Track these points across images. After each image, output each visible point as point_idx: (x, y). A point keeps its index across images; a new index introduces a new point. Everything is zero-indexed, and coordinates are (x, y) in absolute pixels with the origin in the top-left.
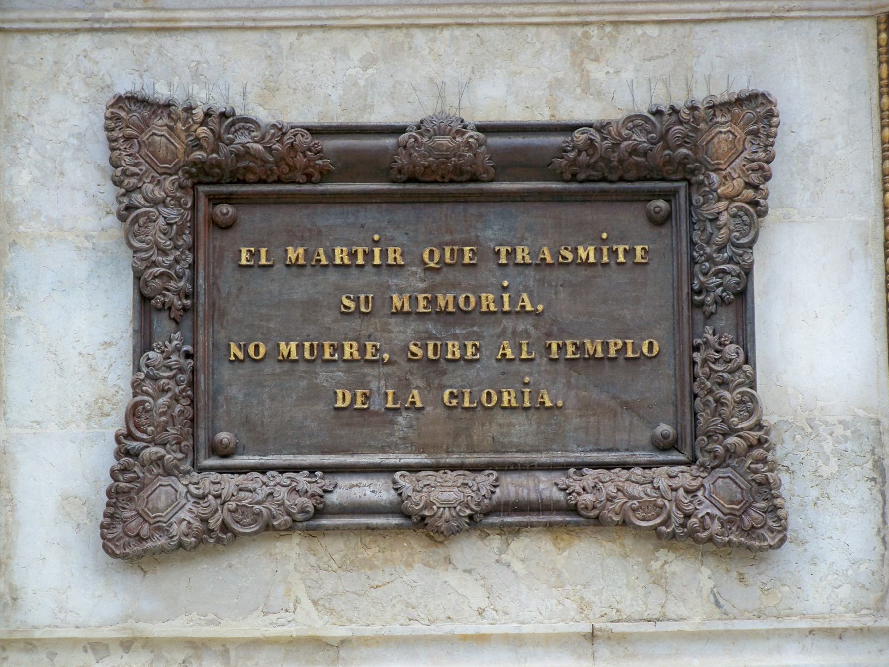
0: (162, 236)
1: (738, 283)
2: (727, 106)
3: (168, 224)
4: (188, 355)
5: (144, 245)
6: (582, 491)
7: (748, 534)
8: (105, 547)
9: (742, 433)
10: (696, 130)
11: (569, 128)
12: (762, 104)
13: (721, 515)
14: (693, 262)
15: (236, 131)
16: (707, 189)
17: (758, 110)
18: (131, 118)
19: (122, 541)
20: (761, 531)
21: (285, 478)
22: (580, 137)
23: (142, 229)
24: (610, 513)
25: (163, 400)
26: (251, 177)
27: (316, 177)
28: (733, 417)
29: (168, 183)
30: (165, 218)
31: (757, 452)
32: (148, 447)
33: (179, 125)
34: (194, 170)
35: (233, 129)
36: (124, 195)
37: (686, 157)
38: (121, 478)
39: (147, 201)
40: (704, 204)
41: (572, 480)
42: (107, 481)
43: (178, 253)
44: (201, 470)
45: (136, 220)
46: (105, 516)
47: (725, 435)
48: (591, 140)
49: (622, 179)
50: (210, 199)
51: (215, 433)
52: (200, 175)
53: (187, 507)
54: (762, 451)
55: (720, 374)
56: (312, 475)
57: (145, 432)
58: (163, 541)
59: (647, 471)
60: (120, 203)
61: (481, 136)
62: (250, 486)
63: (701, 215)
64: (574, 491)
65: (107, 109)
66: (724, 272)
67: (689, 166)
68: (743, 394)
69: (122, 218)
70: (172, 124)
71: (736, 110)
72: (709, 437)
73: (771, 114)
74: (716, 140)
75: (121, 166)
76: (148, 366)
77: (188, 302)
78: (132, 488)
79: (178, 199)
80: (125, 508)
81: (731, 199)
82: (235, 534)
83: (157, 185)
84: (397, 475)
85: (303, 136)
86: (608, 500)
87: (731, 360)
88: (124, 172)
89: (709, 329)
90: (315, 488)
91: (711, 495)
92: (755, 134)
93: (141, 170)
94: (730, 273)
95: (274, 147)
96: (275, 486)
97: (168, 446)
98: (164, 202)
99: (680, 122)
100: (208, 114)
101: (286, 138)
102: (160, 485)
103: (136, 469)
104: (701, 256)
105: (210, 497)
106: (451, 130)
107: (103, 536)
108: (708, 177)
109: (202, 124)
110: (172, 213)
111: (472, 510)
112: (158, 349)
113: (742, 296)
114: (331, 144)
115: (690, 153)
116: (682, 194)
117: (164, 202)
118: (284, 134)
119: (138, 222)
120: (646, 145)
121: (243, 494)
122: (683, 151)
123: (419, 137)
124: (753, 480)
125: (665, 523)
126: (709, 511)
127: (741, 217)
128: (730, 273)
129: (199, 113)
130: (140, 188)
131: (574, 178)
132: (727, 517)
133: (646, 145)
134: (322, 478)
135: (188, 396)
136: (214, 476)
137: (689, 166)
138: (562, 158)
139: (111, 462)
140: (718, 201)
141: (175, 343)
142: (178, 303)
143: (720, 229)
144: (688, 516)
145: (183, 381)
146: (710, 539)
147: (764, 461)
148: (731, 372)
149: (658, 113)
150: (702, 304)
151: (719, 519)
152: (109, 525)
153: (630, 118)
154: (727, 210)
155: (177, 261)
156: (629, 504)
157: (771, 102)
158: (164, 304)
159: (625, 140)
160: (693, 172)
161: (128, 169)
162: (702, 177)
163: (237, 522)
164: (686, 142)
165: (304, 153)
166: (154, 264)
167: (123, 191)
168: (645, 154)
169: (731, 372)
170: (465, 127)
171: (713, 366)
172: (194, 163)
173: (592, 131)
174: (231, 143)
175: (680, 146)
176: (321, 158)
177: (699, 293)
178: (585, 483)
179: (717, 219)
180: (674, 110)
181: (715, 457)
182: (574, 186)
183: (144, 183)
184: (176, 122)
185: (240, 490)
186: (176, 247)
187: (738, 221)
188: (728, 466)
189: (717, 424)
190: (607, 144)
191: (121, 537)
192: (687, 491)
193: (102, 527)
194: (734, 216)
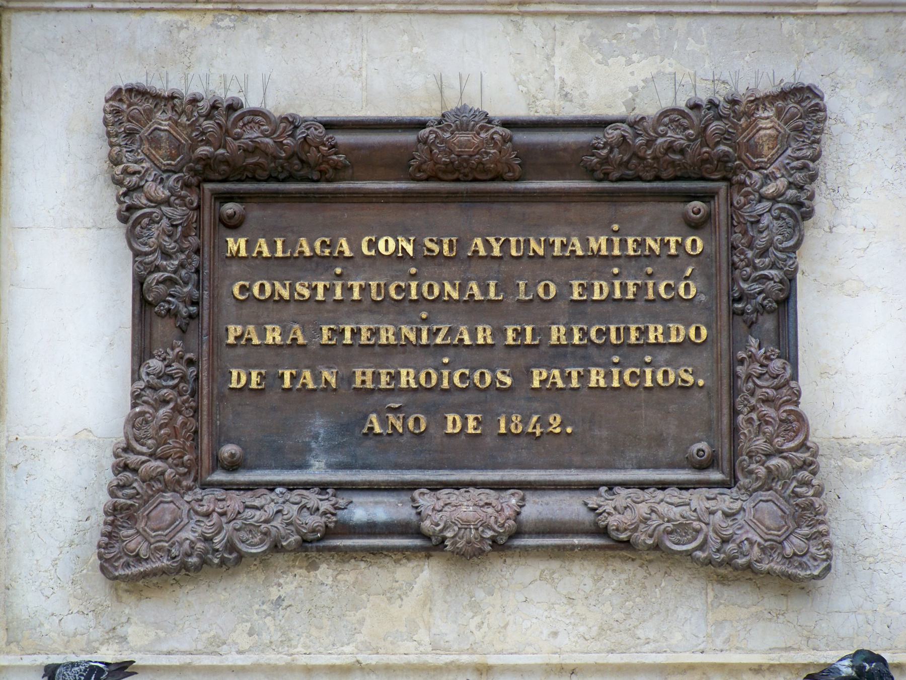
0: (167, 239)
1: (780, 290)
2: (771, 99)
3: (172, 225)
4: (190, 363)
5: (147, 249)
6: (612, 511)
7: (790, 562)
8: (103, 569)
9: (785, 454)
10: (735, 126)
11: (599, 124)
12: (808, 98)
13: (762, 542)
14: (733, 266)
15: (244, 125)
16: (750, 189)
17: (804, 104)
18: (131, 113)
19: (122, 561)
20: (805, 559)
21: (294, 496)
22: (612, 134)
23: (145, 231)
24: (643, 538)
25: (164, 411)
26: (260, 173)
27: (331, 173)
28: (778, 436)
29: (171, 182)
30: (169, 219)
31: (804, 474)
32: (149, 461)
33: (184, 119)
34: (199, 167)
35: (241, 124)
36: (125, 194)
37: (726, 154)
38: (120, 494)
39: (151, 201)
40: (745, 205)
41: (602, 499)
42: (104, 498)
43: (183, 257)
44: (205, 486)
45: (137, 222)
46: (103, 535)
47: (769, 456)
48: (623, 136)
49: (658, 178)
50: (216, 199)
51: (220, 445)
52: (205, 171)
53: (190, 526)
54: (806, 473)
55: (764, 390)
56: (324, 492)
57: (143, 445)
58: (166, 562)
59: (684, 492)
60: (120, 202)
61: (508, 131)
62: (257, 503)
63: (742, 216)
64: (604, 511)
65: (107, 101)
66: (766, 278)
67: (730, 165)
68: (790, 412)
69: (123, 219)
70: (176, 117)
71: (780, 103)
72: (751, 457)
73: (819, 109)
74: (757, 136)
75: (122, 163)
76: (148, 374)
77: (193, 309)
78: (132, 505)
79: (182, 198)
80: (123, 527)
81: (774, 199)
82: (241, 557)
83: (160, 183)
84: (416, 493)
85: (316, 129)
86: (641, 521)
87: (778, 375)
88: (125, 172)
89: (754, 342)
90: (325, 506)
91: (740, 515)
92: (799, 130)
93: (143, 167)
94: (772, 279)
95: (285, 142)
96: (284, 503)
97: (170, 460)
98: (167, 202)
99: (719, 117)
100: (214, 107)
101: (298, 131)
102: (161, 502)
103: (135, 485)
104: (742, 260)
105: (215, 515)
106: (474, 126)
107: (100, 557)
108: (750, 176)
109: (208, 116)
110: (177, 213)
111: (494, 531)
112: (159, 356)
113: (784, 303)
114: (341, 138)
115: (731, 150)
116: (723, 193)
117: (167, 202)
118: (296, 127)
119: (140, 223)
120: (682, 142)
121: (249, 513)
122: (722, 148)
123: (440, 132)
124: (797, 505)
125: (701, 547)
126: (750, 536)
127: (784, 219)
128: (772, 279)
129: (204, 106)
130: (143, 186)
131: (606, 177)
132: (769, 543)
133: (682, 142)
134: (334, 495)
135: (191, 407)
136: (219, 493)
137: (730, 165)
138: (593, 155)
139: (109, 477)
140: (760, 202)
141: (177, 350)
142: (184, 311)
143: (761, 232)
144: (725, 541)
145: (186, 391)
146: (749, 566)
147: (807, 484)
148: (777, 388)
149: (696, 107)
150: (743, 312)
151: (759, 544)
152: (107, 544)
153: (665, 113)
154: (769, 211)
155: (182, 266)
156: (662, 527)
157: (817, 96)
158: (169, 310)
159: (663, 136)
160: (736, 170)
161: (128, 167)
162: (742, 177)
163: (243, 542)
164: (726, 139)
165: (317, 148)
166: (158, 269)
167: (125, 189)
168: (682, 151)
169: (777, 388)
170: (490, 122)
171: (758, 382)
172: (199, 159)
173: (625, 126)
174: (239, 138)
175: (718, 143)
176: (336, 154)
177: (739, 300)
178: (617, 503)
179: (758, 222)
180: (713, 104)
181: (758, 478)
182: (606, 185)
183: (147, 181)
184: (180, 115)
185: (247, 507)
186: (182, 251)
187: (780, 222)
188: (770, 489)
189: (760, 443)
190: (639, 141)
191: (120, 558)
192: (726, 515)
193: (99, 547)
194: (777, 218)
